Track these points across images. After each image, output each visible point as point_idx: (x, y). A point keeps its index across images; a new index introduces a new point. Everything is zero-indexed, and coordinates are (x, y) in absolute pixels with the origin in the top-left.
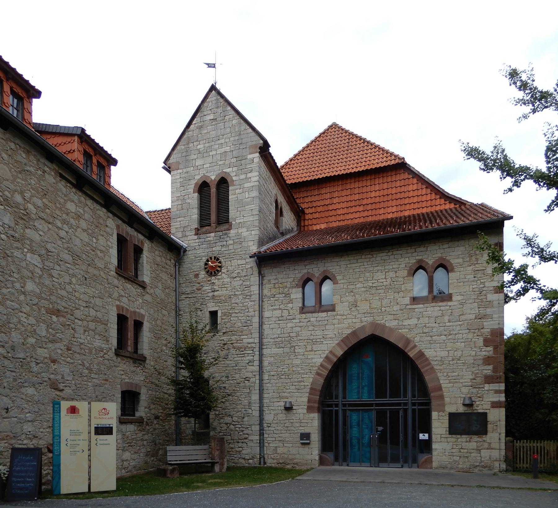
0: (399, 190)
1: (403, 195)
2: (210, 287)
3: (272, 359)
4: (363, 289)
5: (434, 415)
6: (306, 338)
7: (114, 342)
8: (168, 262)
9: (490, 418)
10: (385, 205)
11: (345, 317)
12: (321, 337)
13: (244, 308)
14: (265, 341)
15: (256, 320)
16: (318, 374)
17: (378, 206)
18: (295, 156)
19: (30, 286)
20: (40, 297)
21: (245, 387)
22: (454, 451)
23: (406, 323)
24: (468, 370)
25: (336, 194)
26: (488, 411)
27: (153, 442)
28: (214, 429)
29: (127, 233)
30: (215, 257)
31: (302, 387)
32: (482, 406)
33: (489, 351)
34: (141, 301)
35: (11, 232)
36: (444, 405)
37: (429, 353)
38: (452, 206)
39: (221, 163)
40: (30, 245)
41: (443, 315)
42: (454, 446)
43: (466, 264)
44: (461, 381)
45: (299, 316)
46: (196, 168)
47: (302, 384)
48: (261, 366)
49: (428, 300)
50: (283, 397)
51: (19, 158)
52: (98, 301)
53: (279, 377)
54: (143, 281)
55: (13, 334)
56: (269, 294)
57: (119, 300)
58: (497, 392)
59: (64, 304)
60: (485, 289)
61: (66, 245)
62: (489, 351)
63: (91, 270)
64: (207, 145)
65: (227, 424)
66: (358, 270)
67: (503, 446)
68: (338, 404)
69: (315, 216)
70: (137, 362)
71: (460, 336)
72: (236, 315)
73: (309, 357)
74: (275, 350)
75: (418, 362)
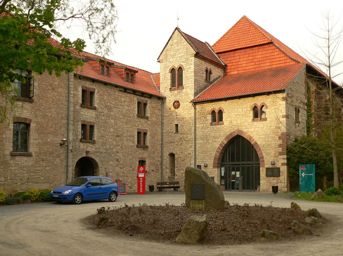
0: (270, 55)
1: (272, 57)
2: (175, 114)
3: (200, 145)
4: (234, 116)
5: (261, 168)
6: (213, 136)
7: (136, 142)
8: (158, 104)
9: (281, 170)
10: (264, 62)
11: (227, 127)
12: (218, 136)
13: (188, 123)
14: (197, 137)
15: (193, 128)
16: (217, 151)
17: (261, 62)
18: (224, 35)
19: (112, 130)
20: (114, 132)
21: (189, 157)
22: (268, 184)
23: (250, 130)
24: (273, 150)
25: (241, 57)
26: (280, 167)
27: (37, 117)
28: (177, 175)
29: (141, 100)
30: (177, 101)
31: (211, 157)
32: (278, 165)
33: (280, 142)
34: (146, 124)
35: (107, 115)
36: (264, 165)
37: (259, 143)
38: (294, 63)
39: (180, 60)
40: (112, 117)
41: (264, 127)
42: (268, 182)
43: (272, 105)
44: (271, 154)
45: (210, 127)
46: (170, 62)
47: (211, 156)
48: (195, 148)
49: (258, 120)
50: (204, 162)
51: (109, 92)
52: (131, 129)
53: (202, 152)
54: (147, 116)
55: (107, 146)
56: (198, 117)
57: (138, 127)
58: (284, 159)
59: (120, 133)
60: (279, 116)
61: (121, 113)
62: (280, 142)
63: (129, 118)
64: (174, 53)
65: (182, 173)
66: (232, 107)
67: (286, 182)
68: (253, 164)
69: (233, 67)
70: (145, 149)
71: (270, 136)
72: (185, 126)
73: (214, 144)
74: (201, 141)
75: (255, 147)
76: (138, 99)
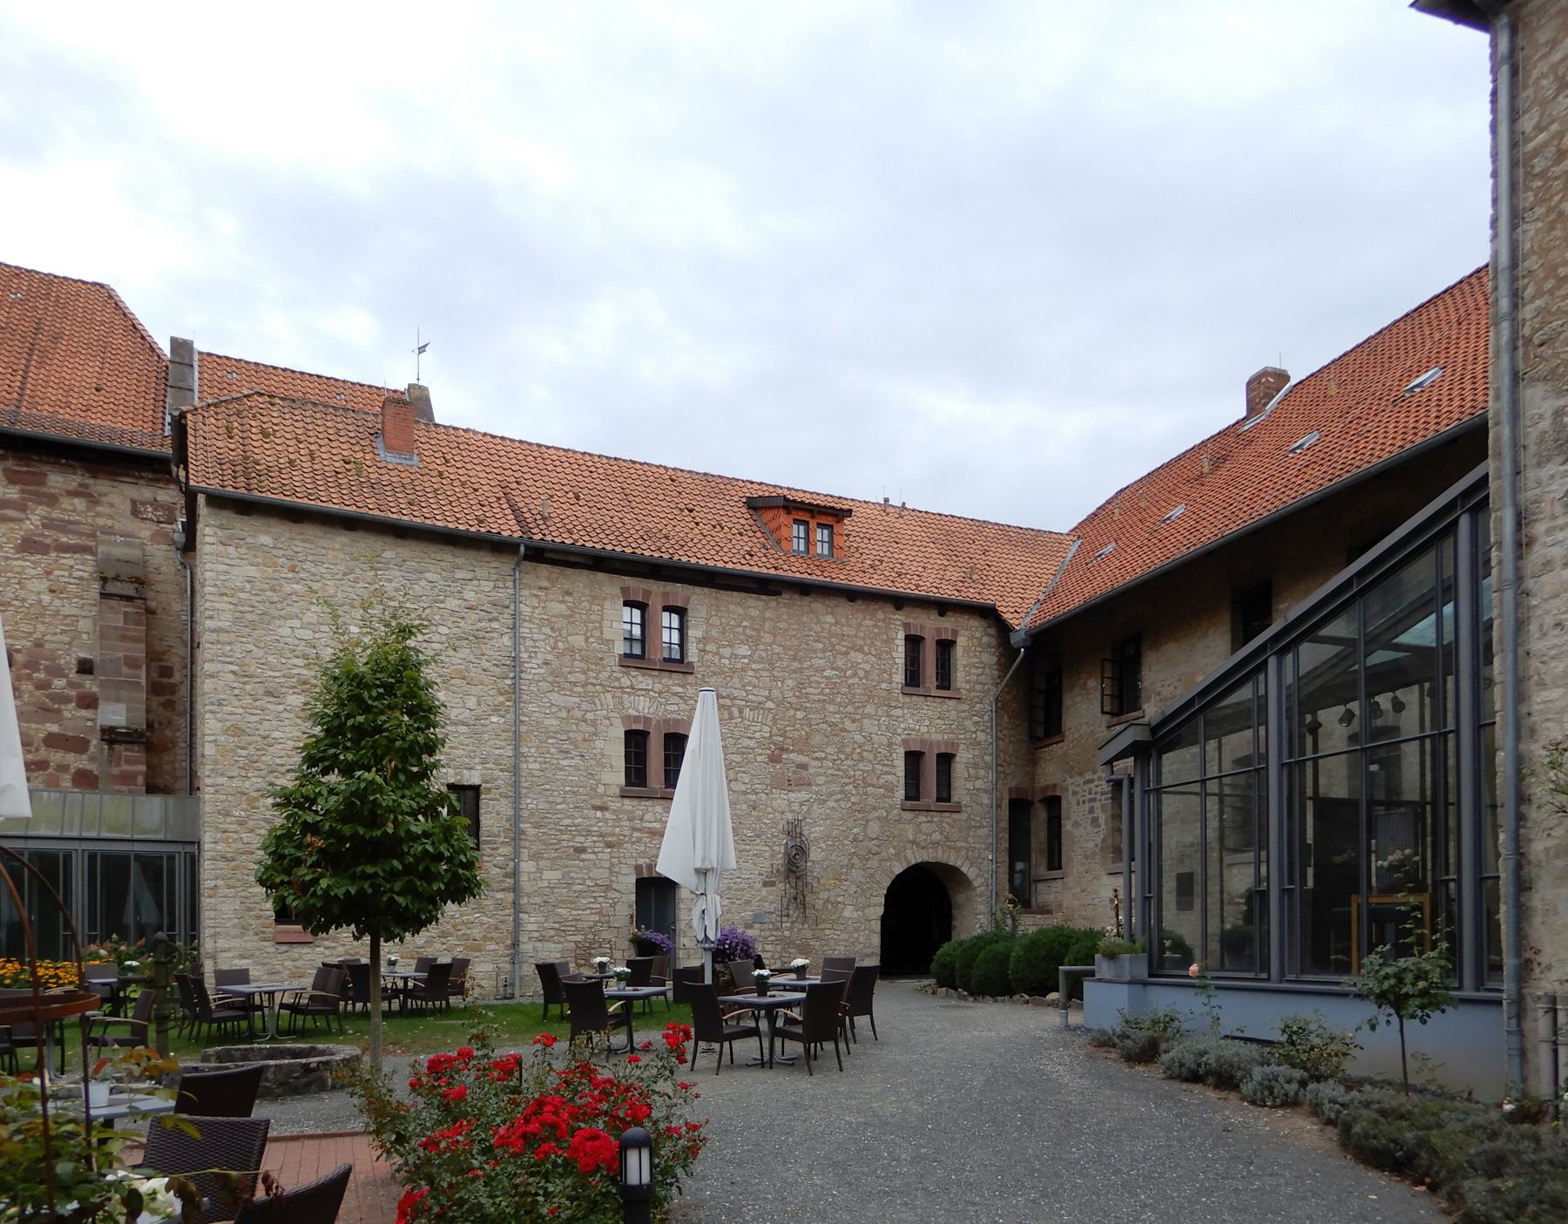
76: (625, 591)
